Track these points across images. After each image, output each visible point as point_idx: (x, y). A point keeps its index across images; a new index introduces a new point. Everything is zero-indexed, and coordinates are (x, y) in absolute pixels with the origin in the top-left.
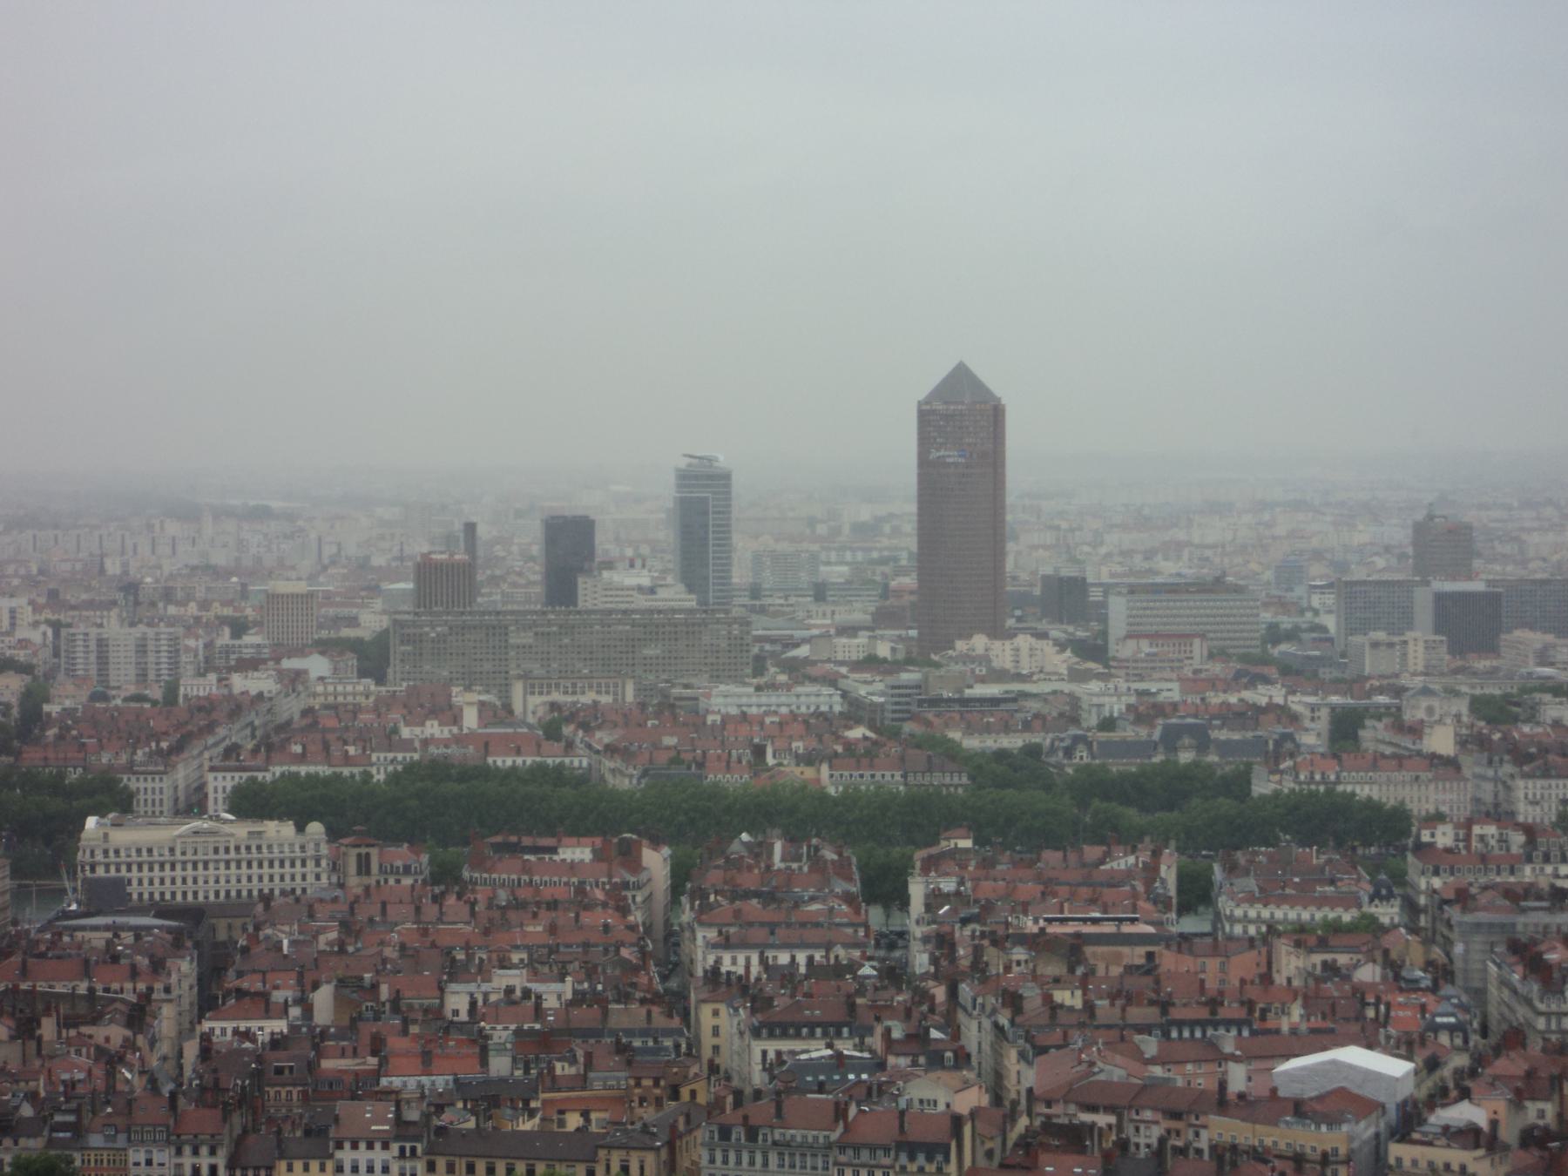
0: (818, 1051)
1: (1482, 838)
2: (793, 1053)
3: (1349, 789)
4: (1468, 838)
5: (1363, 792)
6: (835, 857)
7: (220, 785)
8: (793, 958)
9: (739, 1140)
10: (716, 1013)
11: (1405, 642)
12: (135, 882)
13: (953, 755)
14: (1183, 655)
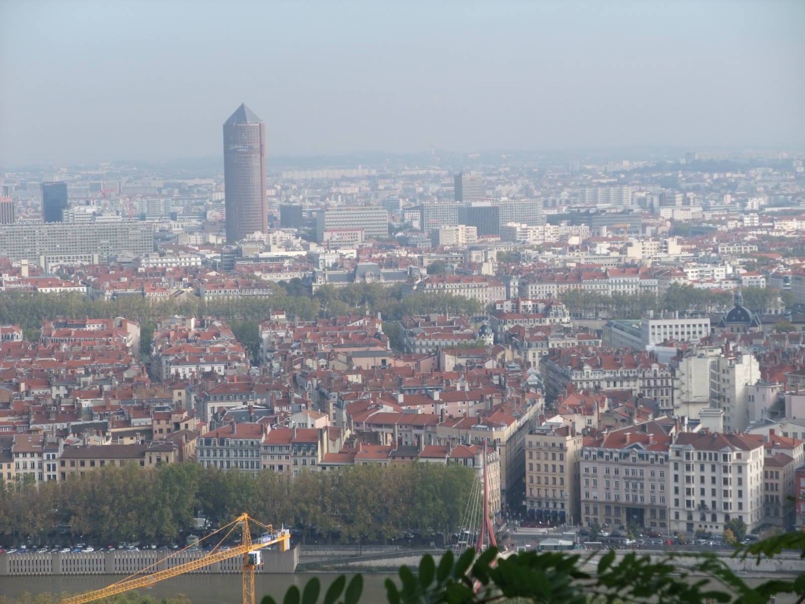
0: (238, 406)
1: (525, 307)
2: (229, 408)
4: (518, 307)
6: (220, 325)
8: (213, 368)
9: (215, 444)
10: (180, 394)
11: (458, 230)
13: (261, 285)
14: (354, 239)
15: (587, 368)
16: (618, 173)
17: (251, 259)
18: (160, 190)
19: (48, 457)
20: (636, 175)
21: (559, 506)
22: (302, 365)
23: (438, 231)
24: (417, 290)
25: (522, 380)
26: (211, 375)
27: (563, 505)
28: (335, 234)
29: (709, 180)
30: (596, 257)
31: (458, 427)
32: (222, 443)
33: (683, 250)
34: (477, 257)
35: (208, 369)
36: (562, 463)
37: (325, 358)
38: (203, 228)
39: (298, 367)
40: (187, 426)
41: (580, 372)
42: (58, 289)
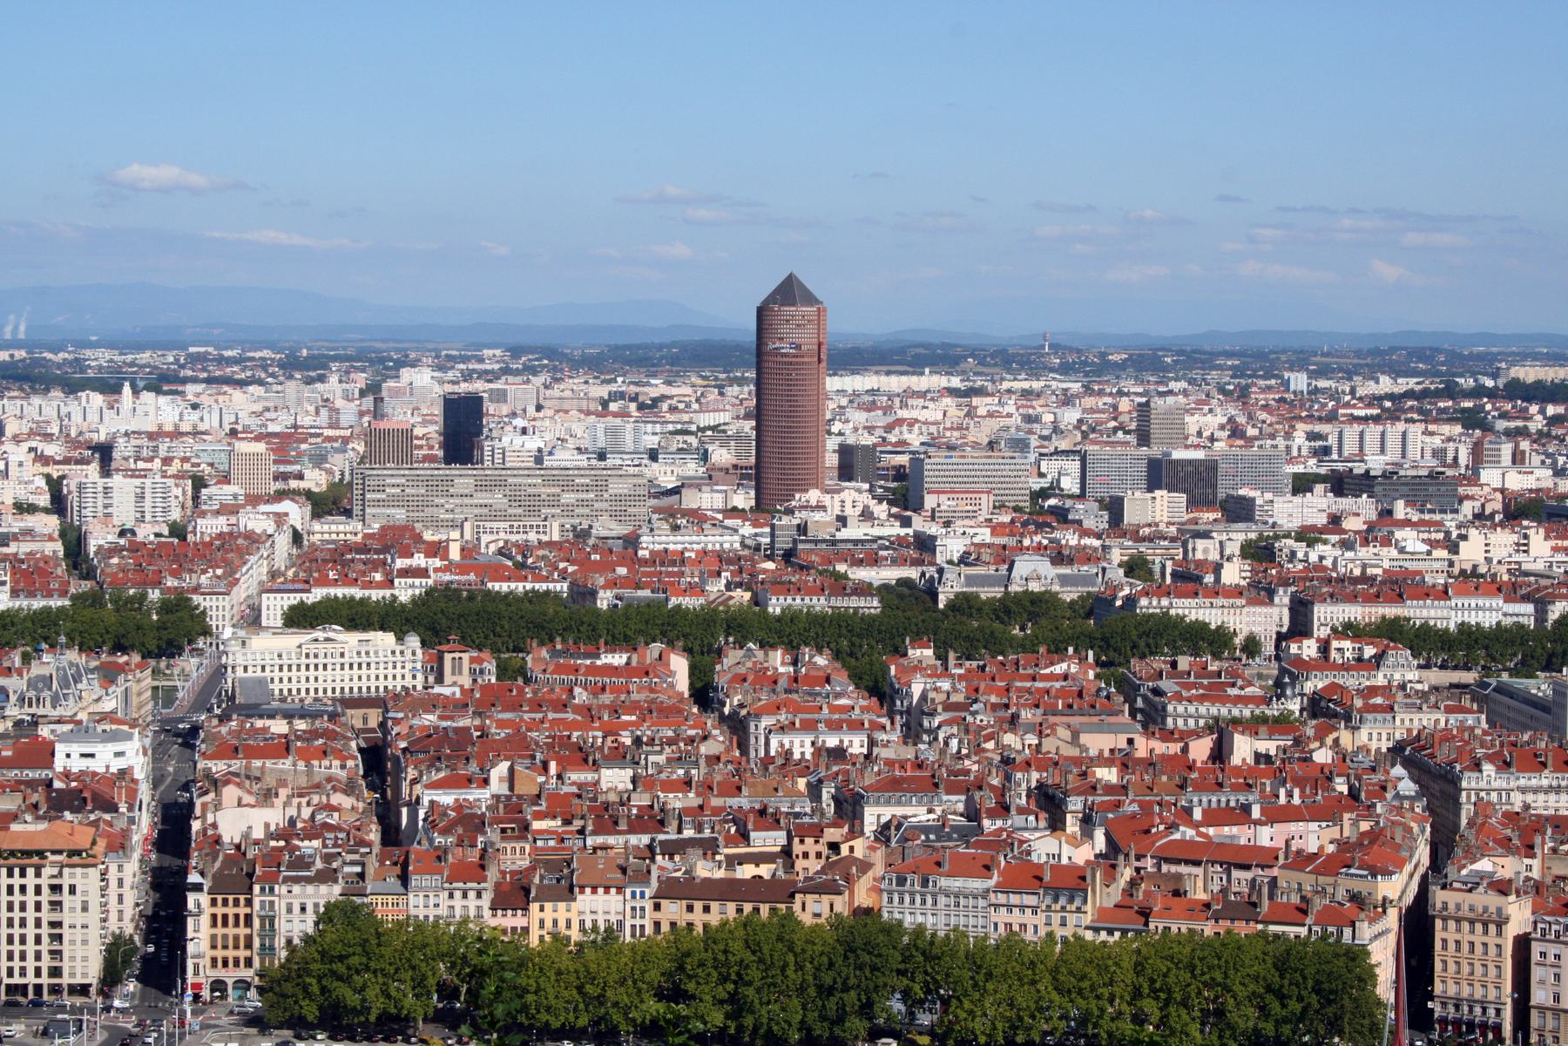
2: (905, 817)
3: (1180, 612)
5: (1193, 616)
7: (275, 607)
12: (277, 680)
15: (1488, 768)
16: (1380, 398)
17: (824, 541)
18: (605, 404)
19: (633, 895)
20: (1410, 403)
21: (1491, 1012)
22: (997, 743)
23: (1122, 499)
24: (1122, 607)
25: (1389, 786)
26: (839, 753)
27: (1498, 1011)
28: (943, 497)
29: (1539, 417)
30: (889, 448)
31: (1316, 872)
32: (925, 883)
33: (1555, 549)
34: (1206, 551)
35: (832, 741)
36: (1498, 941)
37: (1033, 732)
38: (710, 477)
39: (990, 745)
40: (852, 849)
41: (1476, 774)
42: (521, 585)
